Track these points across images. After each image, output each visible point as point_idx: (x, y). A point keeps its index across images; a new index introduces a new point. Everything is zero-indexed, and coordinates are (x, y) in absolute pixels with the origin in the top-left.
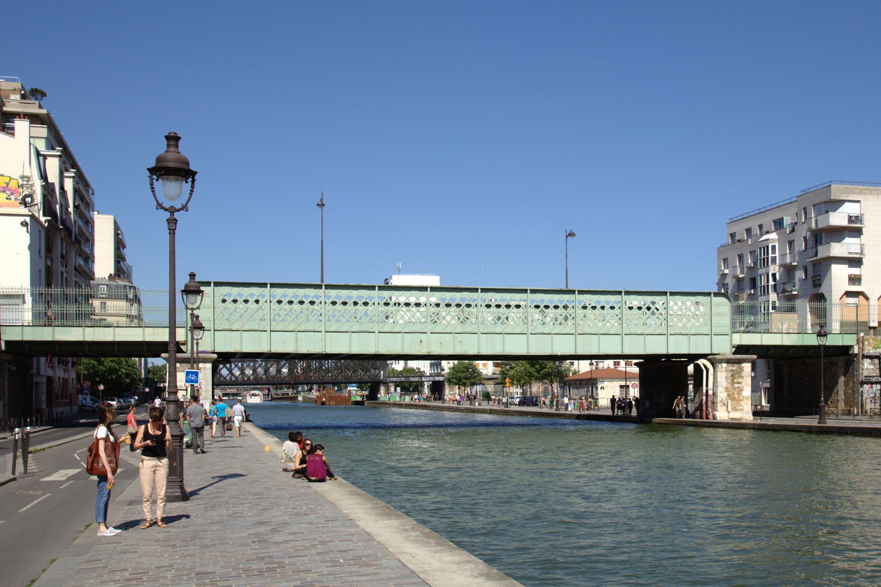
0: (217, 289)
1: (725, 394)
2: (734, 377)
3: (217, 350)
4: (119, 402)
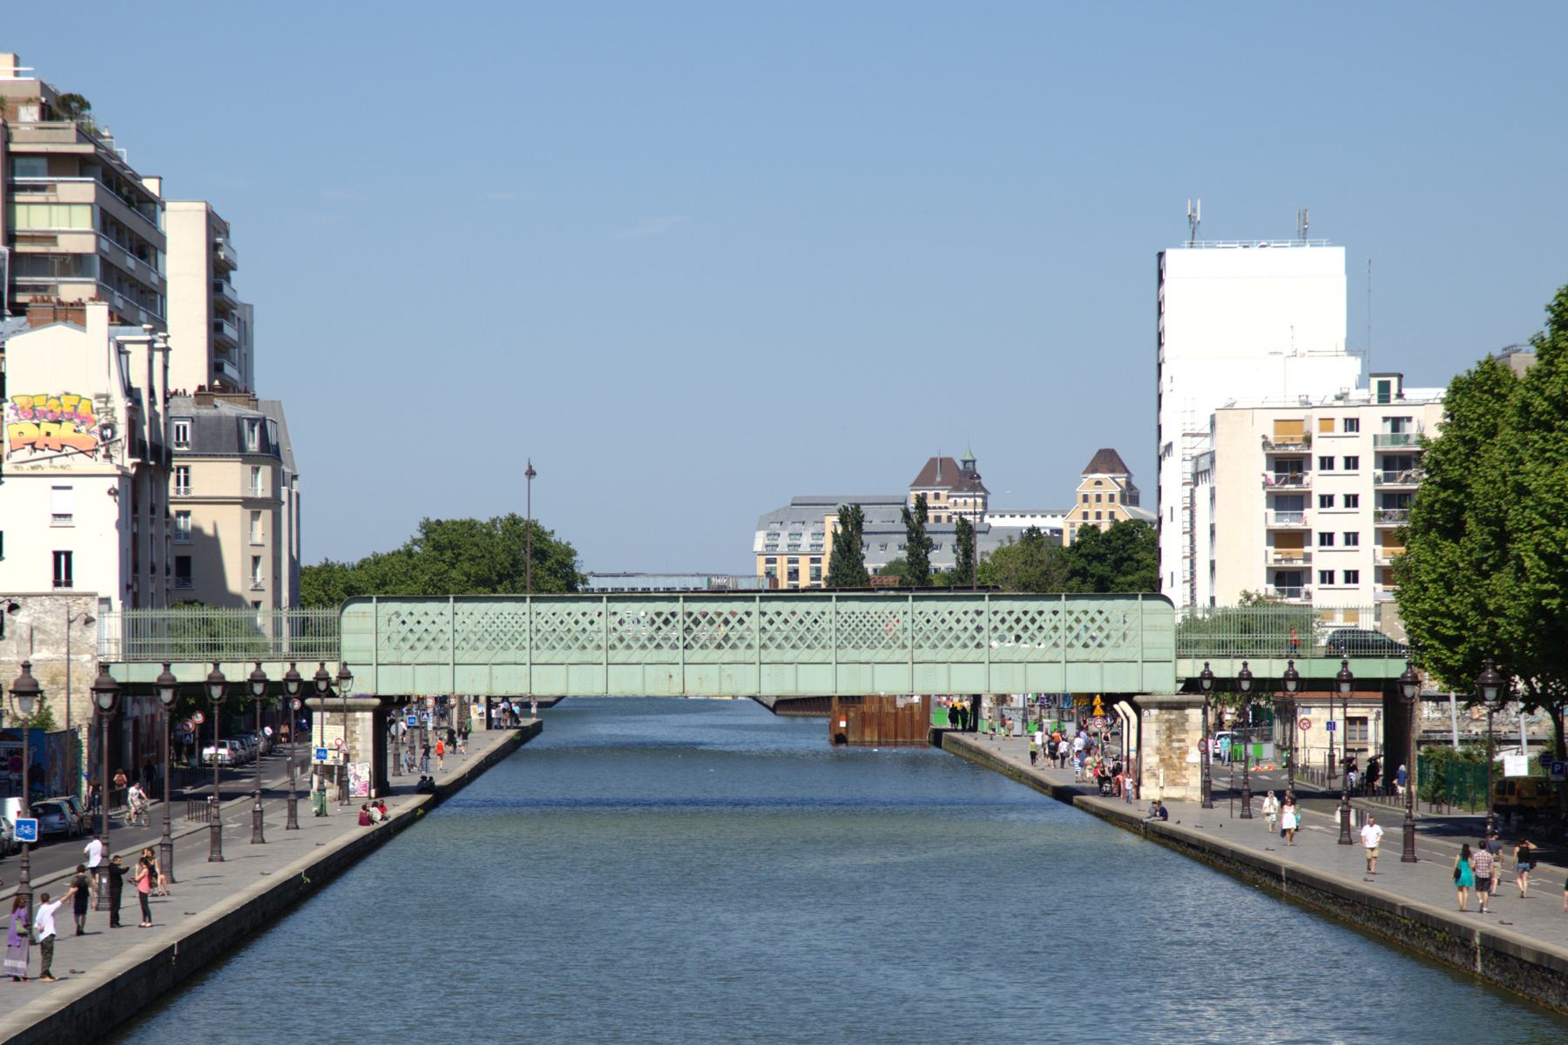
0: (381, 605)
2: (1172, 731)
3: (380, 694)
4: (233, 749)
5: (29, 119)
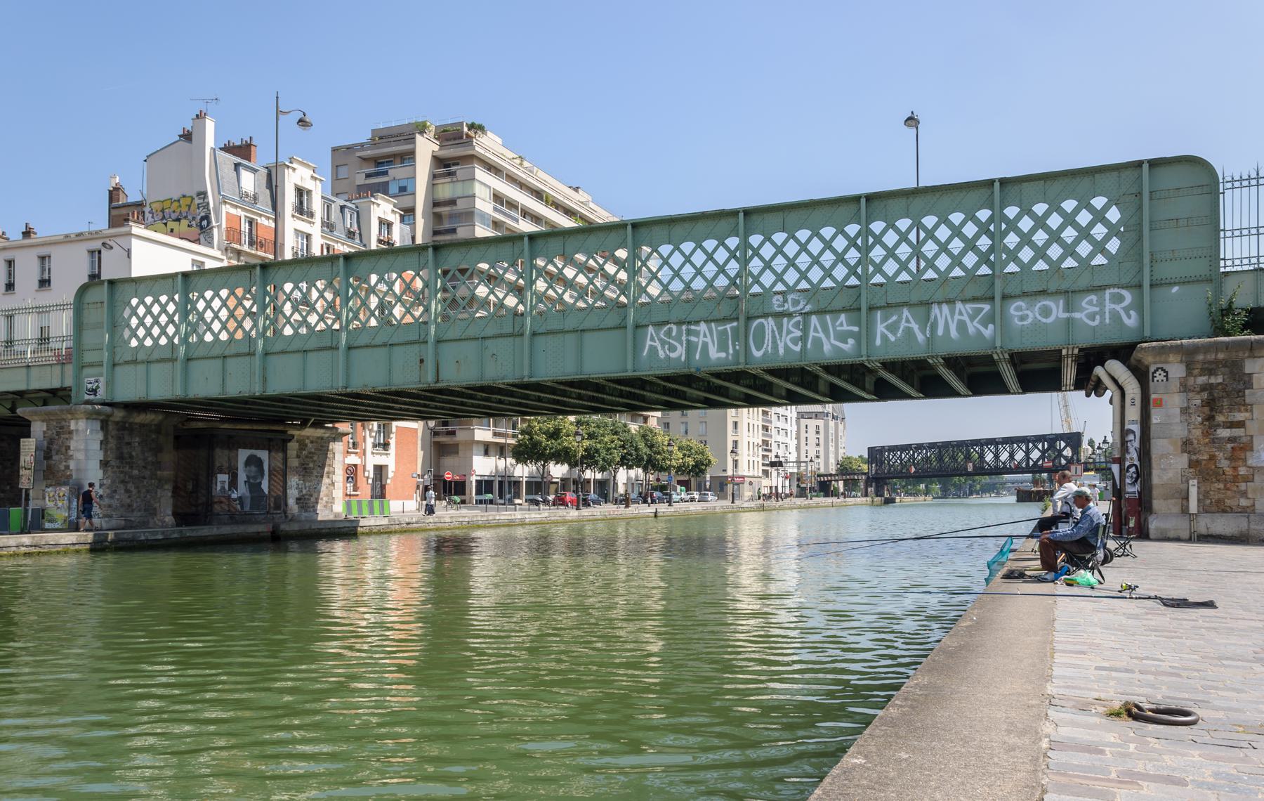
1: (1182, 461)
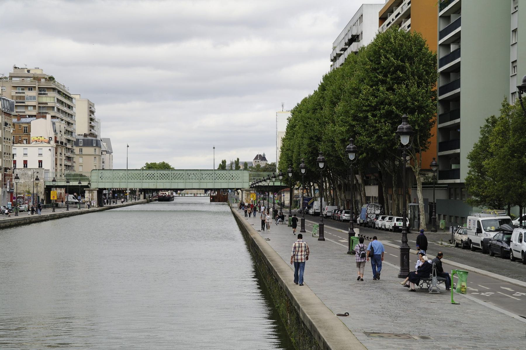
5: (43, 81)
